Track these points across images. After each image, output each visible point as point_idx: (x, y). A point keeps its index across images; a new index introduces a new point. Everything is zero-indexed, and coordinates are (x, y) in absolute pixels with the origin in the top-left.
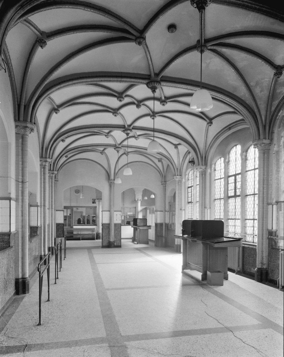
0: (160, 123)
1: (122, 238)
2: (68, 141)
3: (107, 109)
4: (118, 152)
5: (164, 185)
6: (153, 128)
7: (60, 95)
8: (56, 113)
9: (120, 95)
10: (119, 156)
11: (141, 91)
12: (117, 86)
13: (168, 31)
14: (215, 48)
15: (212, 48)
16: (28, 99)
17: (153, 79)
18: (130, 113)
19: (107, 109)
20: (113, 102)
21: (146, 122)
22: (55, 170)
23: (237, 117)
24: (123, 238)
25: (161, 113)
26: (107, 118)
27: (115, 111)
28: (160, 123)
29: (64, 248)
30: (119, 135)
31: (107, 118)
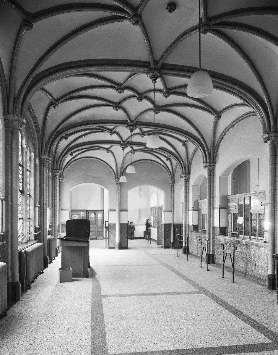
0: (164, 117)
1: (157, 229)
2: (71, 138)
3: (108, 103)
4: (124, 149)
5: (173, 184)
6: (153, 122)
7: (56, 86)
8: (54, 107)
9: (120, 87)
10: (124, 155)
11: (143, 80)
12: (119, 76)
13: (167, 8)
14: (215, 28)
15: (215, 28)
16: (17, 93)
17: (157, 67)
18: (136, 107)
19: (108, 103)
20: (112, 94)
21: (149, 117)
22: (58, 168)
23: (248, 109)
24: (136, 237)
25: (166, 108)
26: (109, 112)
27: (117, 105)
28: (164, 117)
29: (190, 211)
30: (125, 132)
31: (109, 112)
